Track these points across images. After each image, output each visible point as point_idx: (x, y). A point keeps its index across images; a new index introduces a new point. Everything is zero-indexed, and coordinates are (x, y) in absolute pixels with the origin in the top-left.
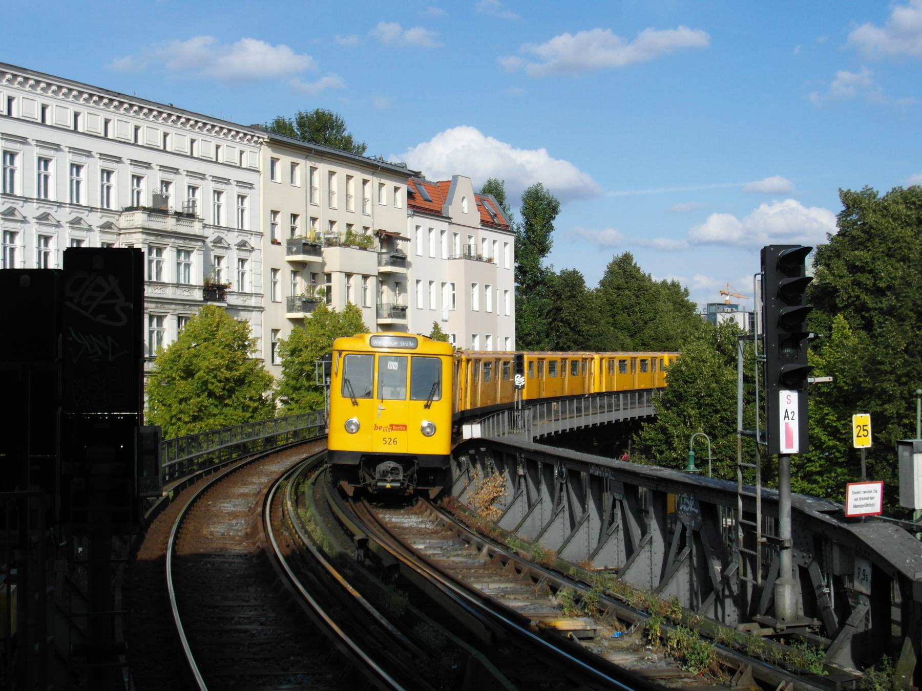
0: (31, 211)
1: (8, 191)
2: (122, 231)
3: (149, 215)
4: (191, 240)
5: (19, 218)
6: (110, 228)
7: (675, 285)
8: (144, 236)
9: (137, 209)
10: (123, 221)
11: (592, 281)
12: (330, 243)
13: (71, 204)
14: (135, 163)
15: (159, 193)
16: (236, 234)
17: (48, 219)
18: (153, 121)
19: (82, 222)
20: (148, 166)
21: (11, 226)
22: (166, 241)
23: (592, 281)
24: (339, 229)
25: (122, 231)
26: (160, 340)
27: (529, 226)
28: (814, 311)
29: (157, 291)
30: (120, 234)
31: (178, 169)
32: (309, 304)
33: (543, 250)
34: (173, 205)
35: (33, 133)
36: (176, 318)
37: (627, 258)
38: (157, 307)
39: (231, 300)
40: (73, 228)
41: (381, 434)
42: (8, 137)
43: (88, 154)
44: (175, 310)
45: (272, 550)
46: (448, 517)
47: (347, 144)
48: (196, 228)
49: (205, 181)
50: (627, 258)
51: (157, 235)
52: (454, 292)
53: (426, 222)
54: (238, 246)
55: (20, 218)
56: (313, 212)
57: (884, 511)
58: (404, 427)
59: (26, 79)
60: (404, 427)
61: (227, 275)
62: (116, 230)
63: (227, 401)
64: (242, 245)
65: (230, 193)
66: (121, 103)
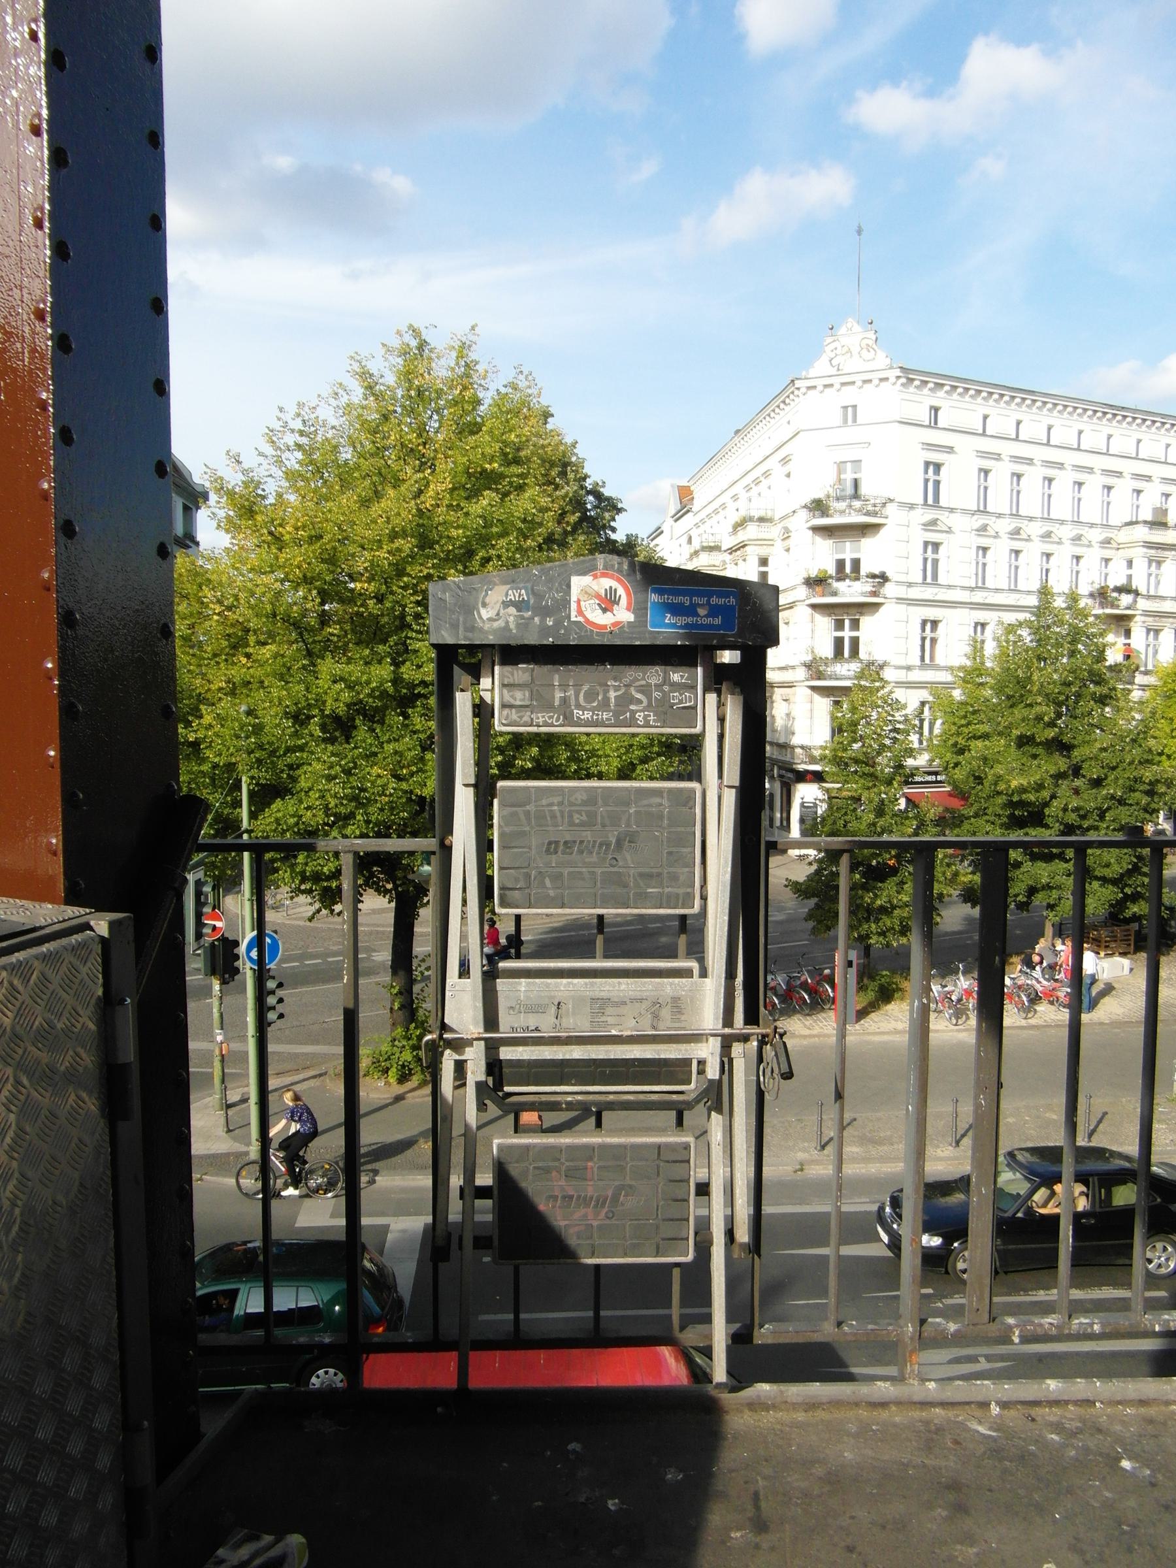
0: (1035, 529)
1: (1014, 512)
2: (1121, 546)
3: (1150, 529)
4: (1163, 549)
5: (1024, 536)
6: (1109, 543)
8: (1145, 550)
9: (1137, 523)
10: (1122, 536)
13: (1011, 515)
14: (1107, 472)
15: (1159, 506)
16: (1007, 520)
17: (1050, 537)
18: (1155, 433)
19: (1052, 535)
20: (1148, 478)
21: (984, 542)
22: (1167, 553)
25: (1121, 546)
26: (1156, 652)
29: (1156, 605)
30: (1118, 549)
31: (1063, 464)
35: (1008, 449)
36: (1145, 630)
38: (1155, 621)
40: (1074, 545)
42: (930, 447)
43: (1090, 470)
44: (1172, 623)
46: (569, 915)
49: (1064, 471)
51: (1157, 548)
52: (1129, 572)
54: (924, 525)
55: (1025, 537)
57: (456, 1349)
59: (1034, 401)
62: (1115, 545)
63: (971, 709)
65: (1094, 484)
66: (1125, 417)
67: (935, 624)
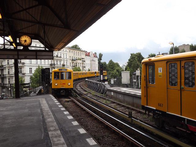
7: (117, 63)
11: (107, 63)
12: (77, 60)
23: (107, 63)
24: (78, 58)
27: (100, 57)
28: (96, 58)
32: (74, 67)
33: (101, 60)
34: (59, 56)
35: (63, 52)
37: (111, 60)
39: (65, 66)
41: (61, 85)
45: (127, 99)
47: (79, 49)
48: (61, 59)
50: (111, 60)
53: (87, 57)
56: (74, 56)
58: (65, 84)
60: (65, 84)
61: (65, 64)
64: (66, 60)
67: (31, 69)
